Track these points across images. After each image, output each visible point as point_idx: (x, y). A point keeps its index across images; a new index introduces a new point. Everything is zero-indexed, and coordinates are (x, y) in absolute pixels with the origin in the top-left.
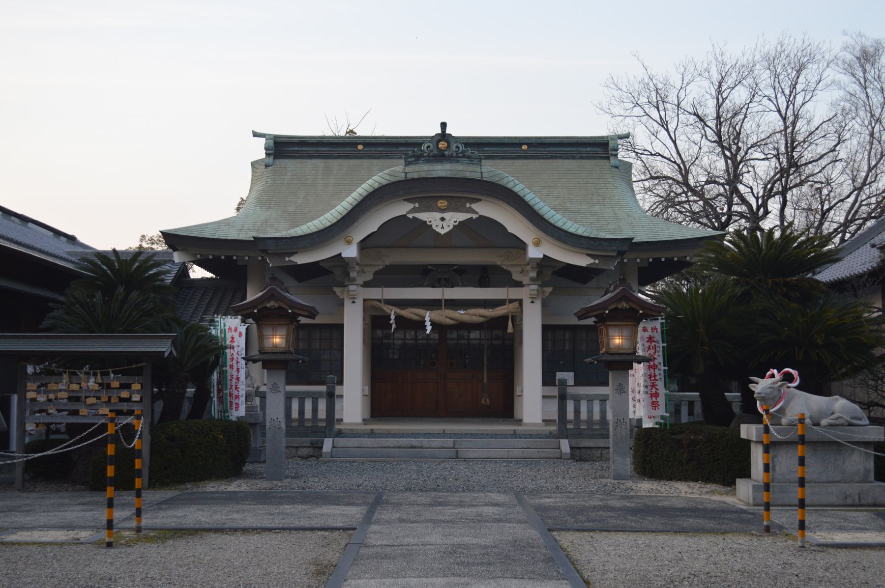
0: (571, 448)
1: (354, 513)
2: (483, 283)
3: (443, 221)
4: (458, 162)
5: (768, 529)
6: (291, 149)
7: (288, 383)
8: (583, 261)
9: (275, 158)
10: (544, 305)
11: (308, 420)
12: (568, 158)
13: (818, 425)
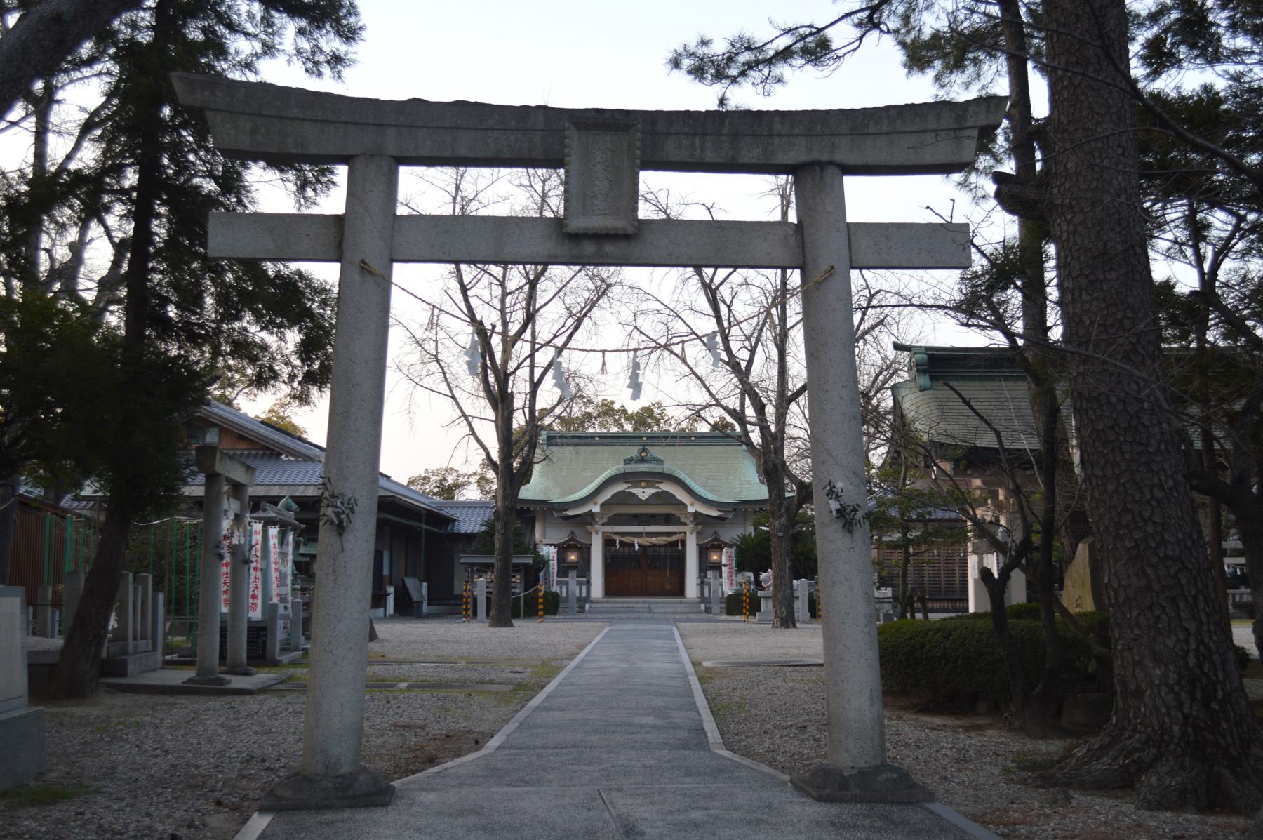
3: (644, 493)
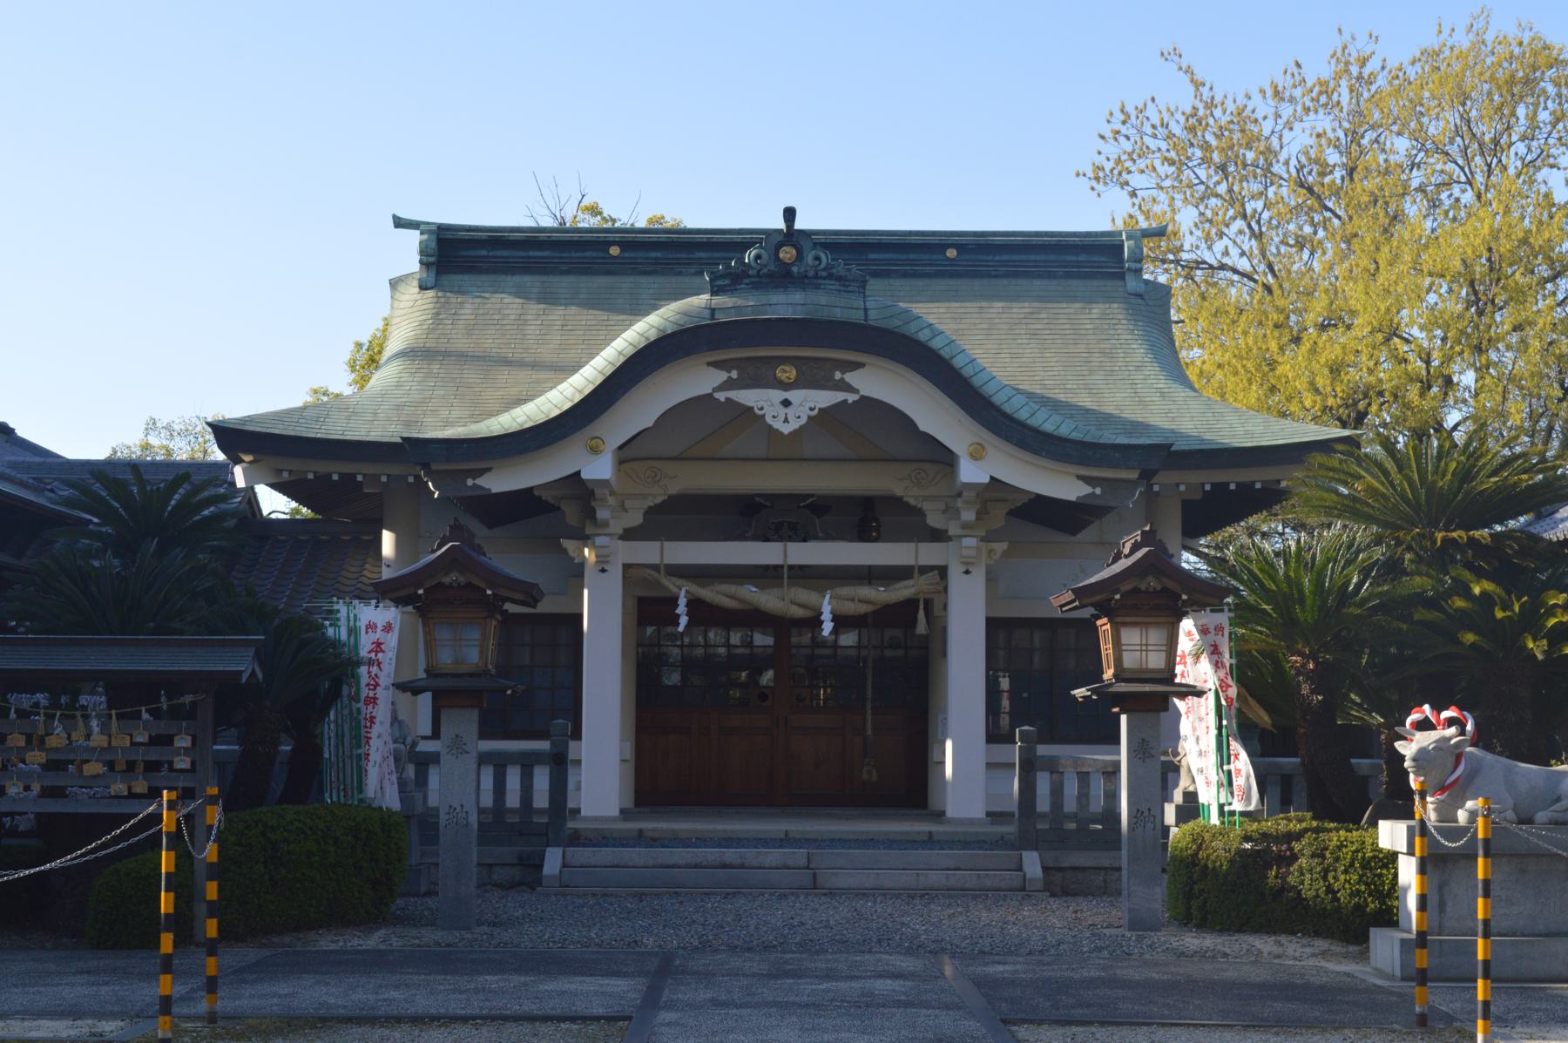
0: (1045, 869)
1: (623, 990)
2: (865, 532)
3: (787, 408)
4: (817, 287)
5: (1423, 1020)
6: (473, 253)
7: (483, 735)
8: (1065, 487)
9: (438, 273)
10: (991, 579)
11: (513, 811)
12: (1039, 276)
13: (1530, 821)
